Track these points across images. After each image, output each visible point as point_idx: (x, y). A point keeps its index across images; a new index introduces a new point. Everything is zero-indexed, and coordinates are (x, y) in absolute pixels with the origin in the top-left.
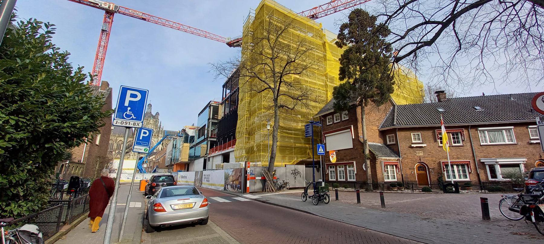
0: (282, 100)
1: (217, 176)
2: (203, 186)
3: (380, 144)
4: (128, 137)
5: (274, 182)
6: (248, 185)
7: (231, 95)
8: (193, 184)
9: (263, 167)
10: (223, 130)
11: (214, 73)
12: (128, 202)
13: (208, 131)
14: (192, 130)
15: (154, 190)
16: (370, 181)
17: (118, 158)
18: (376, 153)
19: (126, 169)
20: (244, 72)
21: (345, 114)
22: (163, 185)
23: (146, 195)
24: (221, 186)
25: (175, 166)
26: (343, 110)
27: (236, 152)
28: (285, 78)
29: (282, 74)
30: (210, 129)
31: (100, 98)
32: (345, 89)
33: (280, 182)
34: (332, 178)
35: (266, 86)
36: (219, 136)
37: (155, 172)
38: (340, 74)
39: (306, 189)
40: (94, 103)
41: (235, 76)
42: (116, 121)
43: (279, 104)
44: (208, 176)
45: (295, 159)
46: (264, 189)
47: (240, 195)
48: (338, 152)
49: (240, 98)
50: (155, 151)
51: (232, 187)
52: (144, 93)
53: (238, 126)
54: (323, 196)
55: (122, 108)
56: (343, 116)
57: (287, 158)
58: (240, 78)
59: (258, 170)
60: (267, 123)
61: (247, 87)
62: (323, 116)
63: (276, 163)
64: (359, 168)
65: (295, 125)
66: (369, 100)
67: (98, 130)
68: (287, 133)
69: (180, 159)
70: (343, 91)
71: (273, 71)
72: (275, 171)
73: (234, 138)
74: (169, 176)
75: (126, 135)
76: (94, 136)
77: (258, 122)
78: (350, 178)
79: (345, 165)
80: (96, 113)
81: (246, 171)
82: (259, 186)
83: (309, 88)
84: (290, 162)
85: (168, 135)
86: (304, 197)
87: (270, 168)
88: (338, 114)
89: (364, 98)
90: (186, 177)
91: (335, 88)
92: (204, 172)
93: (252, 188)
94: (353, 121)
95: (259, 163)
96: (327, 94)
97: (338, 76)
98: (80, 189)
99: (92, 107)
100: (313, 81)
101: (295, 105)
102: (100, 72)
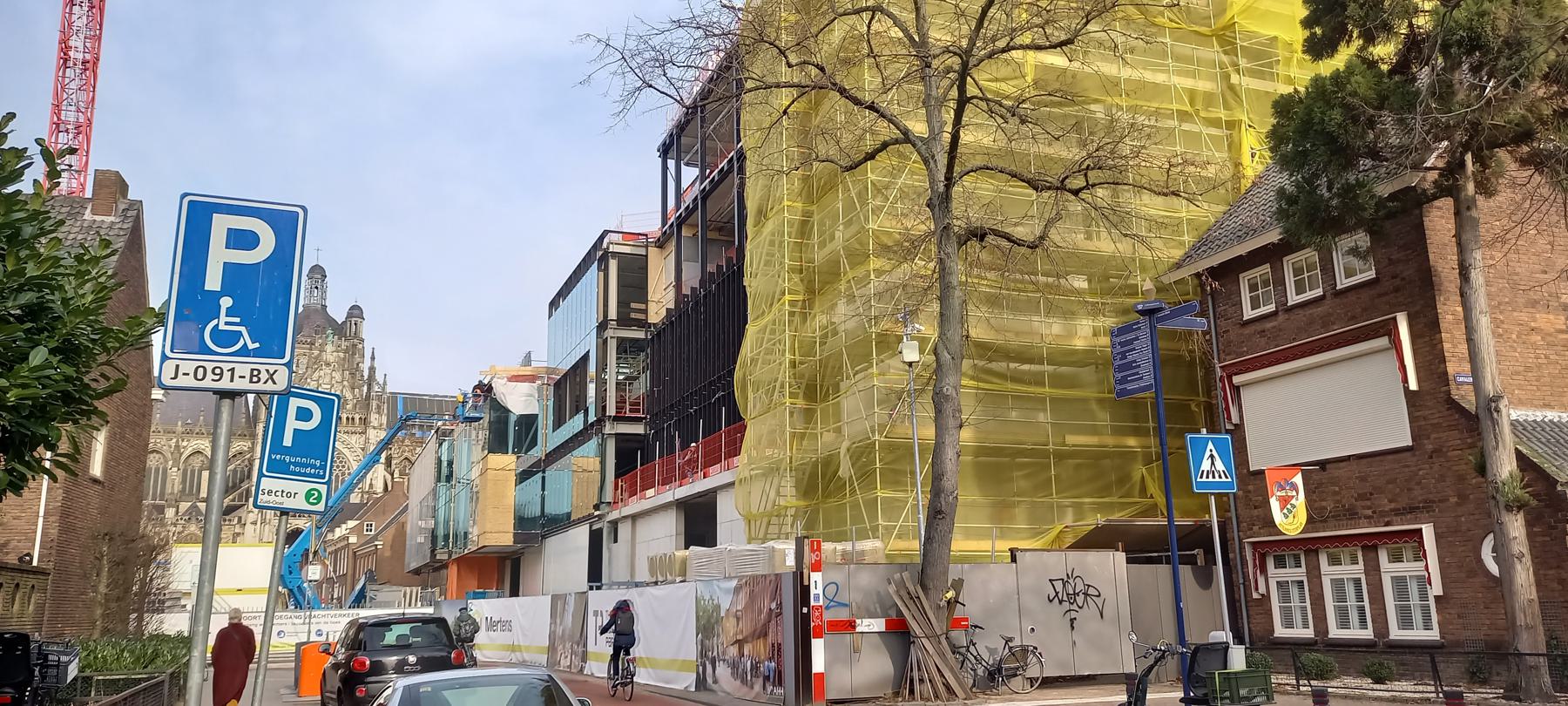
0: (977, 197)
5: (955, 649)
6: (818, 665)
7: (705, 195)
8: (543, 659)
10: (673, 376)
11: (613, 82)
13: (601, 384)
19: (229, 592)
20: (760, 65)
21: (1354, 251)
22: (401, 669)
25: (453, 571)
26: (1337, 226)
27: (751, 485)
28: (985, 78)
29: (965, 55)
30: (612, 376)
32: (1347, 108)
33: (988, 647)
35: (886, 131)
36: (658, 409)
37: (360, 600)
38: (1307, 23)
40: (70, 286)
41: (720, 90)
42: (169, 362)
43: (958, 225)
45: (1069, 519)
48: (1320, 474)
49: (751, 206)
52: (286, 224)
55: (194, 301)
57: (1020, 512)
58: (747, 98)
59: (866, 579)
60: (900, 330)
61: (785, 146)
62: (1214, 272)
66: (1502, 154)
67: (96, 411)
68: (1017, 378)
69: (474, 532)
70: (1337, 115)
71: (920, 46)
72: (958, 585)
73: (736, 419)
74: (426, 621)
76: (82, 439)
77: (851, 324)
78: (1406, 622)
79: (1370, 545)
80: (85, 333)
81: (805, 590)
83: (1125, 117)
84: (1036, 534)
85: (413, 417)
87: (928, 569)
88: (1309, 255)
90: (506, 625)
91: (1283, 106)
94: (1406, 288)
95: (868, 545)
96: (1234, 147)
97: (1299, 35)
98: (35, 692)
99: (65, 302)
100: (1149, 76)
101: (1050, 223)
102: (83, 129)
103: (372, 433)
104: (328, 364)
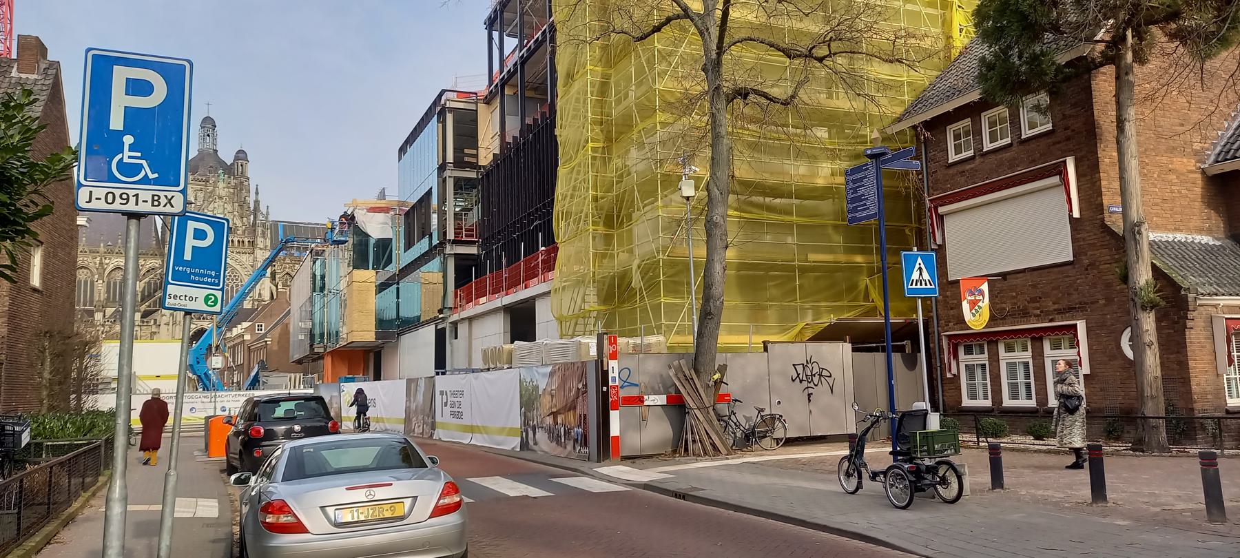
0: (742, 63)
1: (489, 395)
2: (439, 434)
3: (1206, 239)
4: (138, 256)
5: (720, 417)
6: (615, 430)
7: (523, 61)
9: (674, 352)
10: (503, 209)
12: (169, 498)
14: (381, 217)
15: (257, 453)
16: (1154, 407)
17: (110, 337)
18: (1187, 279)
21: (1037, 108)
22: (289, 435)
23: (231, 470)
24: (511, 432)
25: (328, 361)
26: (1025, 88)
27: (562, 294)
30: (451, 208)
31: (20, 107)
33: (745, 416)
34: (973, 396)
36: (487, 234)
37: (255, 384)
39: (857, 443)
44: (454, 394)
46: (680, 446)
47: (585, 466)
48: (1002, 283)
49: (561, 69)
50: (247, 305)
51: (553, 436)
52: (175, 75)
53: (561, 188)
54: (933, 470)
55: (102, 140)
56: (1024, 117)
59: (652, 367)
60: (679, 171)
62: (928, 125)
63: (724, 339)
64: (1105, 351)
65: (803, 170)
66: (1155, 29)
67: (28, 231)
69: (344, 331)
72: (723, 369)
73: (550, 241)
74: (307, 399)
75: (132, 245)
77: (641, 167)
79: (1036, 337)
81: (605, 374)
82: (658, 430)
84: (784, 330)
85: (290, 241)
86: (848, 475)
87: (700, 358)
88: (1002, 111)
89: (1128, 23)
92: (440, 380)
93: (634, 441)
95: (653, 339)
96: (947, 23)
101: (800, 85)
103: (258, 253)
104: (221, 198)
